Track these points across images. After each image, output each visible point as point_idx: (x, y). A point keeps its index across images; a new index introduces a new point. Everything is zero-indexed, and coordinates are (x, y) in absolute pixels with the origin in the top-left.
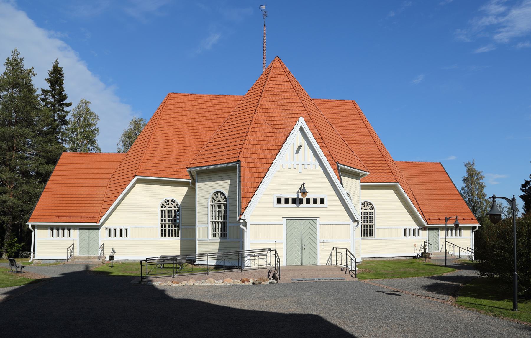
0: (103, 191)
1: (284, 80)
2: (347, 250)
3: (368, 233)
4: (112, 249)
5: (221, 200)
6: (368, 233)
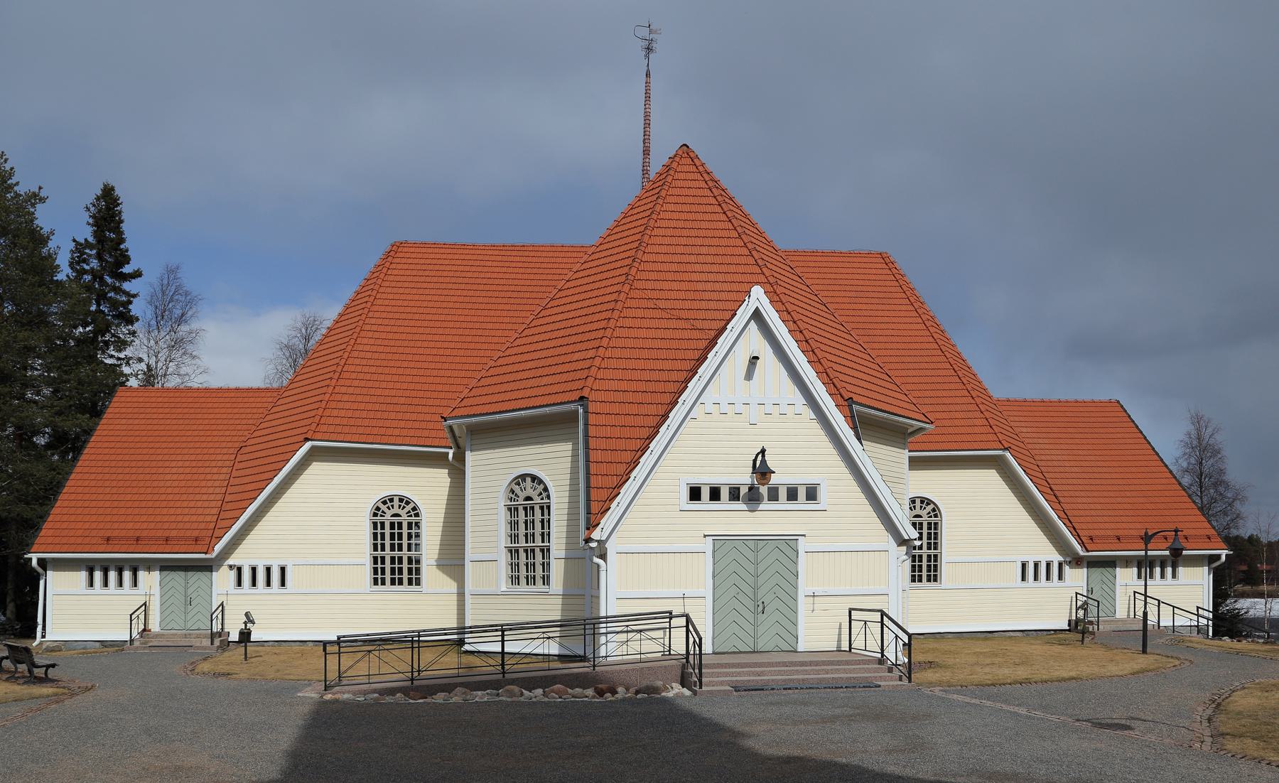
0: (222, 477)
1: (705, 200)
2: (883, 614)
3: (924, 573)
4: (247, 615)
5: (534, 494)
6: (924, 573)
